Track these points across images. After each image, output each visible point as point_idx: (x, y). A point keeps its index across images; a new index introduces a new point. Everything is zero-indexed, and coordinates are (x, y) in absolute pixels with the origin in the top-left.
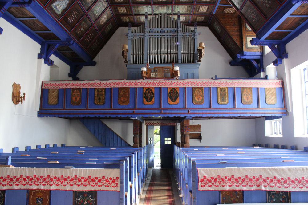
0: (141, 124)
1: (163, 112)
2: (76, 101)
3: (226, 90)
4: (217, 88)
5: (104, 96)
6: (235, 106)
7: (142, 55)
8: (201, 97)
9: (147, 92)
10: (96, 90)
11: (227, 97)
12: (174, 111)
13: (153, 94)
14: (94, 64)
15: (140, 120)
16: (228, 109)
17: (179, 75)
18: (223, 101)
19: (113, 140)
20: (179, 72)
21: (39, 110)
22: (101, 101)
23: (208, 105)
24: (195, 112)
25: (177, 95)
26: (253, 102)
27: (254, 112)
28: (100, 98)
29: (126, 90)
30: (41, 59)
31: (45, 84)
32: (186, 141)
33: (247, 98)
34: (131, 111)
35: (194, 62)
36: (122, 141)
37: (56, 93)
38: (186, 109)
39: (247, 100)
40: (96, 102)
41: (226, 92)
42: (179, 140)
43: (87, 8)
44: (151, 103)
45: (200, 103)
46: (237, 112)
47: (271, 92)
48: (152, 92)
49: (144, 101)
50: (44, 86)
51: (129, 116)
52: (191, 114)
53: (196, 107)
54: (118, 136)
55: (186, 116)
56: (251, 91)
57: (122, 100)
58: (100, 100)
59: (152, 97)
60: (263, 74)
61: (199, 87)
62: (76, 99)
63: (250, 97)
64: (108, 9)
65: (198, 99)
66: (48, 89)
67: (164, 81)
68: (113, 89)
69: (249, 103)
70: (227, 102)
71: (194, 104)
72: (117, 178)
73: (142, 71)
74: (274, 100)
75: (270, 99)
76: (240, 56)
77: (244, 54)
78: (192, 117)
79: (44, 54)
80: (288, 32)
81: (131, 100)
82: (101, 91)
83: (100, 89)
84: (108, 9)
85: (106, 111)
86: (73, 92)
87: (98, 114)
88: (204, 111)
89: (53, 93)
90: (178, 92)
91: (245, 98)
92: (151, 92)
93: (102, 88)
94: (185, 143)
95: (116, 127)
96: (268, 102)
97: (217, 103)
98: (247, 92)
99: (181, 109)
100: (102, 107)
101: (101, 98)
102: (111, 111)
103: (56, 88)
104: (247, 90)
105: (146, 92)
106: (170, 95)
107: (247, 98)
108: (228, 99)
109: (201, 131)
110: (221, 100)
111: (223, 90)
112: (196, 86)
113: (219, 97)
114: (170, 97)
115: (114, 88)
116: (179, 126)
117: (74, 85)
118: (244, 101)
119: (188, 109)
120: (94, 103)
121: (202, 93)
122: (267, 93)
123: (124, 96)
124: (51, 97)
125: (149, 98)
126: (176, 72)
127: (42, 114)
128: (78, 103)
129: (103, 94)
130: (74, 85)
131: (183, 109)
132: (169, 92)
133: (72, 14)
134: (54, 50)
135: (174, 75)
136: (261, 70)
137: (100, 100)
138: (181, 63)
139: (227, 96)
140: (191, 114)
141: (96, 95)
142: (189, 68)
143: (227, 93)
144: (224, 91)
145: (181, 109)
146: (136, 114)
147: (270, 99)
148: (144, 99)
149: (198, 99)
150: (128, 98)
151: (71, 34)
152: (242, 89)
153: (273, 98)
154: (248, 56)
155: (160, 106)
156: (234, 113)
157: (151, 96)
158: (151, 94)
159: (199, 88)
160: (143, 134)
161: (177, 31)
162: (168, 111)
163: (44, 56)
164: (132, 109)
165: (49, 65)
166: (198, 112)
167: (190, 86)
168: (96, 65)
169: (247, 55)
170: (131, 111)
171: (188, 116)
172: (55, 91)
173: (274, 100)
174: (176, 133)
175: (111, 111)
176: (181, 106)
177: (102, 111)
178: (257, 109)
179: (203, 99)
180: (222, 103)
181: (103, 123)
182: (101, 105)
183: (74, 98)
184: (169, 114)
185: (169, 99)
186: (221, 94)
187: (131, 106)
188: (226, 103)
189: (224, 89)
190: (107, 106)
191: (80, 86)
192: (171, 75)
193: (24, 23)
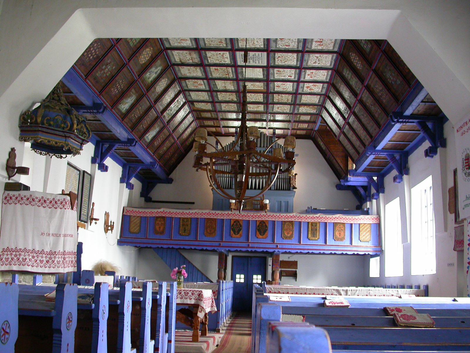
0: (226, 256)
1: (250, 246)
2: (159, 230)
3: (318, 225)
4: (308, 223)
5: (189, 226)
6: (326, 242)
7: (230, 179)
8: (291, 232)
9: (235, 224)
10: (181, 220)
11: (318, 233)
12: (261, 246)
13: (241, 226)
14: (170, 181)
15: (225, 253)
16: (318, 245)
17: (268, 208)
18: (314, 237)
19: (193, 275)
20: (268, 206)
21: (119, 238)
22: (186, 231)
23: (297, 240)
24: (284, 247)
25: (266, 228)
26: (346, 239)
27: (346, 249)
28: (185, 228)
29: (213, 221)
30: (123, 184)
31: (127, 210)
32: (275, 277)
33: (340, 234)
34: (217, 244)
35: (289, 190)
36: (203, 277)
37: (137, 221)
38: (275, 244)
39: (340, 236)
40: (180, 232)
41: (318, 227)
42: (269, 278)
43: (173, 129)
44: (238, 236)
45: (289, 238)
46: (328, 248)
47: (365, 229)
48: (240, 224)
49: (231, 234)
50: (126, 213)
51: (216, 248)
52: (280, 248)
53: (285, 241)
54: (198, 270)
55: (275, 251)
56: (345, 226)
57: (209, 231)
58: (185, 230)
59: (240, 230)
60: (369, 203)
61: (289, 221)
62: (160, 228)
63: (342, 233)
64: (190, 115)
65: (288, 234)
66: (130, 216)
67: (251, 214)
68: (199, 219)
69: (342, 239)
70: (318, 237)
71: (283, 239)
72: (216, 291)
73: (231, 203)
74: (368, 237)
75: (364, 235)
76: (345, 182)
77: (349, 180)
78: (280, 252)
79: (98, 157)
80: (381, 168)
81: (218, 232)
82: (187, 221)
83: (185, 218)
84: (190, 115)
85: (191, 243)
86: (156, 220)
87: (183, 245)
88: (293, 247)
89: (135, 221)
90: (267, 225)
91: (337, 233)
92: (238, 224)
93: (187, 218)
94: (274, 280)
95: (196, 260)
96: (362, 239)
97: (308, 238)
98: (340, 228)
99: (269, 243)
100: (187, 238)
101: (187, 228)
102: (197, 243)
103: (138, 215)
104: (340, 225)
105: (233, 224)
106: (258, 228)
107: (340, 234)
108: (319, 235)
109: (297, 269)
110: (312, 235)
111: (314, 225)
112: (286, 220)
113: (310, 232)
114: (259, 230)
115: (200, 218)
116: (270, 261)
117: (159, 213)
118: (336, 238)
119: (276, 244)
120: (179, 233)
121: (292, 227)
122: (361, 229)
123: (211, 227)
124: (132, 225)
125: (236, 231)
126: (266, 204)
127: (122, 242)
128: (162, 233)
129: (189, 224)
130: (159, 213)
131: (271, 243)
132: (257, 225)
133: (117, 83)
134: (136, 173)
135: (263, 207)
136: (368, 199)
137: (185, 230)
138: (274, 189)
139: (318, 231)
140: (280, 248)
141: (181, 226)
142: (282, 197)
143: (318, 228)
144: (316, 225)
145: (269, 243)
146: (223, 247)
147: (364, 235)
148: (231, 231)
149: (288, 234)
150: (215, 230)
151: (154, 156)
152: (335, 224)
153: (367, 234)
154: (354, 182)
155: (248, 240)
156: (324, 250)
157: (239, 228)
158: (239, 226)
159: (289, 221)
160: (227, 269)
161: (271, 152)
162: (256, 245)
163: (98, 160)
164: (218, 242)
165: (129, 189)
166: (287, 247)
167: (280, 220)
168: (173, 182)
169: (352, 180)
170: (217, 244)
171: (276, 250)
172: (137, 218)
173: (368, 237)
174: (267, 268)
175: (197, 243)
176: (269, 240)
177: (187, 243)
178: (350, 246)
179: (292, 234)
180: (313, 238)
181: (181, 254)
182: (186, 236)
183: (157, 227)
184: (257, 248)
185: (258, 232)
186: (312, 229)
187: (217, 238)
188: (317, 238)
189: (316, 224)
190: (192, 237)
191: (166, 214)
192: (260, 207)
193: (117, 153)
